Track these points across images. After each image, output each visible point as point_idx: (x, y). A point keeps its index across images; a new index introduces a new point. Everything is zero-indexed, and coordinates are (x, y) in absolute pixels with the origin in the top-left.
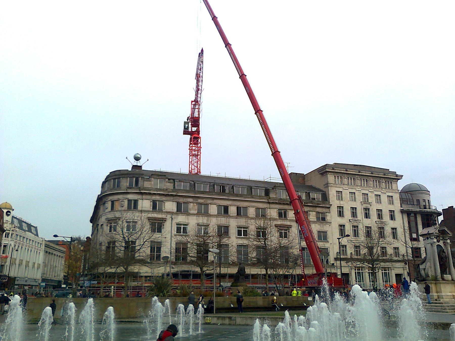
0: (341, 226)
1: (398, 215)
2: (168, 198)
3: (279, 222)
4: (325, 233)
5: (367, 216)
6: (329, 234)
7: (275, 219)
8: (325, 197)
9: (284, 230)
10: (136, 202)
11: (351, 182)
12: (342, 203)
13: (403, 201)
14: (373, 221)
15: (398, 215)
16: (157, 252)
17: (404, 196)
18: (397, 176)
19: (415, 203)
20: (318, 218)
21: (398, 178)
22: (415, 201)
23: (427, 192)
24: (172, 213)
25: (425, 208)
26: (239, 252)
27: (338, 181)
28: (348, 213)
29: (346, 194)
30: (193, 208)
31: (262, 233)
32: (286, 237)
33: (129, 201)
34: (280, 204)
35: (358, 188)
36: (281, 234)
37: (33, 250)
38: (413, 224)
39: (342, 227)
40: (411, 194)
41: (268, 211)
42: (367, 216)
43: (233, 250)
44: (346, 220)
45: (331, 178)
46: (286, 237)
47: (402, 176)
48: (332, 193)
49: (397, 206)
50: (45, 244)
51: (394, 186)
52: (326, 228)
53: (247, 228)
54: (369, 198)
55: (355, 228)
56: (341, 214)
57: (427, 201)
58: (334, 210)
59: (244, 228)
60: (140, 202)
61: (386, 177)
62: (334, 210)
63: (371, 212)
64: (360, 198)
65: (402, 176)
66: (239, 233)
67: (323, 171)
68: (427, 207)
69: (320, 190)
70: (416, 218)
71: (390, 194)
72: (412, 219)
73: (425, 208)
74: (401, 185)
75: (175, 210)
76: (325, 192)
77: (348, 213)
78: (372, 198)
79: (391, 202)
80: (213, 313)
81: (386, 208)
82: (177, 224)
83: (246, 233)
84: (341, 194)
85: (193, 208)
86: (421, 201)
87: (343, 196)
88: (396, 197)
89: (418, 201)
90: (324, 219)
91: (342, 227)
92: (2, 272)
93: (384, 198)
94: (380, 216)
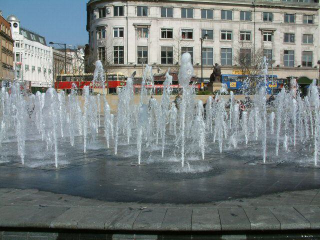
3: (264, 26)
4: (311, 36)
6: (282, 40)
7: (258, 23)
9: (269, 33)
10: (121, 8)
16: (117, 58)
20: (304, 21)
24: (157, 19)
26: (222, 55)
31: (246, 36)
32: (270, 39)
33: (115, 8)
34: (265, 7)
36: (265, 37)
37: (43, 57)
41: (253, 15)
43: (217, 52)
46: (270, 39)
50: (53, 52)
53: (231, 32)
60: (125, 8)
75: (159, 16)
80: (166, 16)
82: (162, 29)
84: (192, 54)
90: (311, 22)
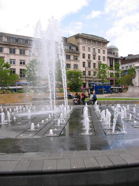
0: (83, 62)
1: (106, 58)
2: (5, 46)
5: (94, 58)
8: (77, 49)
11: (84, 42)
12: (84, 52)
13: (109, 53)
14: (96, 61)
15: (106, 58)
17: (109, 51)
18: (107, 41)
19: (113, 54)
21: (108, 42)
22: (113, 53)
23: (117, 49)
24: (8, 54)
25: (116, 56)
27: (83, 41)
28: (87, 57)
29: (86, 48)
30: (18, 51)
35: (86, 45)
38: (111, 62)
39: (84, 63)
40: (111, 50)
42: (94, 58)
44: (86, 60)
45: (80, 41)
47: (109, 42)
48: (81, 47)
49: (106, 55)
51: (106, 47)
52: (77, 63)
54: (96, 50)
55: (89, 63)
56: (84, 57)
57: (117, 54)
58: (81, 55)
59: (23, 60)
61: (104, 42)
62: (81, 55)
63: (96, 57)
64: (92, 50)
65: (109, 42)
66: (21, 63)
67: (77, 37)
68: (117, 56)
69: (76, 46)
70: (113, 60)
71: (104, 49)
72: (111, 60)
73: (116, 56)
74: (108, 45)
76: (77, 47)
77: (87, 57)
78: (97, 51)
79: (104, 53)
81: (102, 55)
83: (24, 63)
85: (18, 51)
86: (115, 53)
87: (85, 49)
88: (106, 51)
89: (114, 53)
90: (77, 59)
91: (84, 63)
92: (30, 128)
93: (101, 51)
94: (89, 58)
